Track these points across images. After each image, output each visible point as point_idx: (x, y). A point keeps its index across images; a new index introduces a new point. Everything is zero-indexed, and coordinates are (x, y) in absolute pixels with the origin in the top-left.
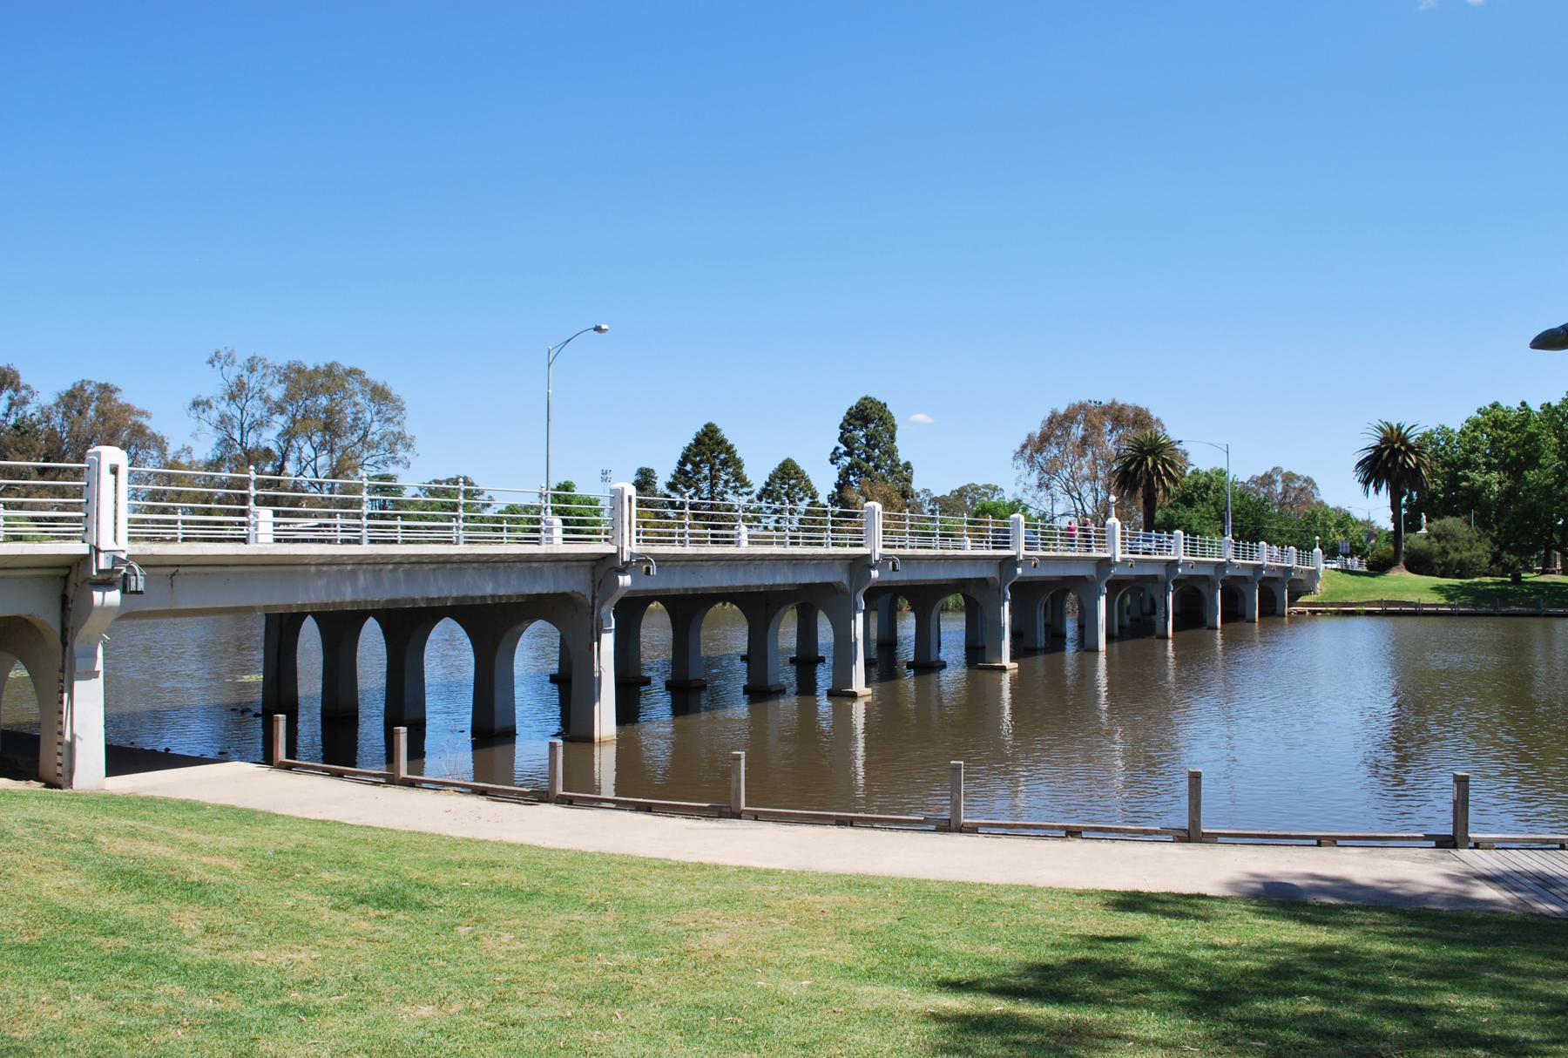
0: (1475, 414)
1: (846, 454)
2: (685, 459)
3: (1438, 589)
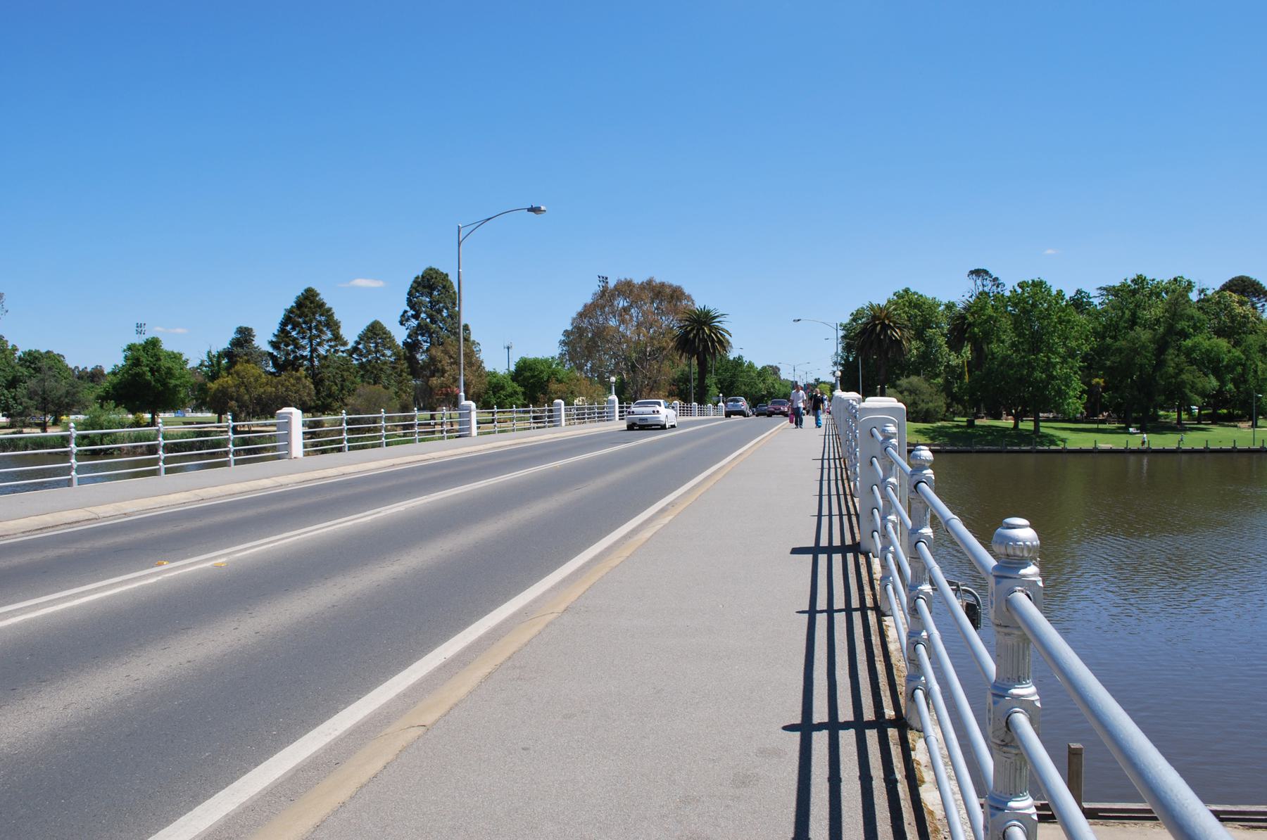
0: (891, 296)
1: (413, 316)
2: (287, 320)
3: (919, 431)
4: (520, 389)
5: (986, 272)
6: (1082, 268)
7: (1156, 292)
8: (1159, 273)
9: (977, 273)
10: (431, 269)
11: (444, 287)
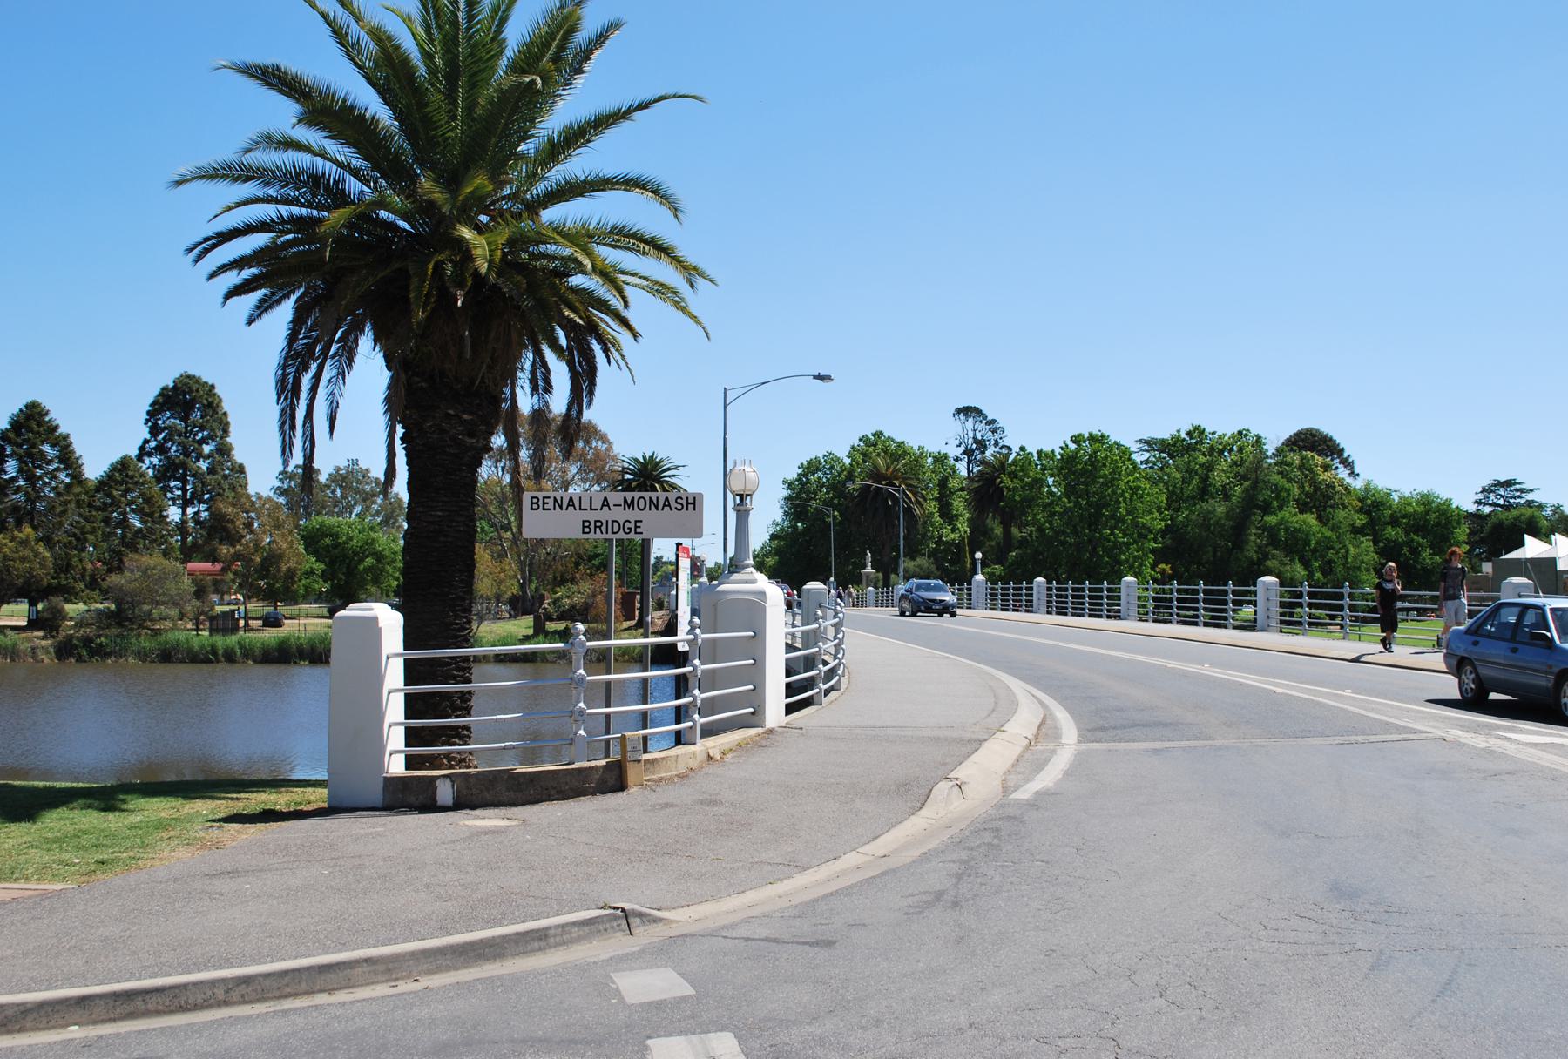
4: (319, 567)
5: (977, 411)
6: (1136, 419)
7: (1219, 449)
8: (1221, 425)
9: (966, 411)
10: (189, 377)
11: (210, 405)
